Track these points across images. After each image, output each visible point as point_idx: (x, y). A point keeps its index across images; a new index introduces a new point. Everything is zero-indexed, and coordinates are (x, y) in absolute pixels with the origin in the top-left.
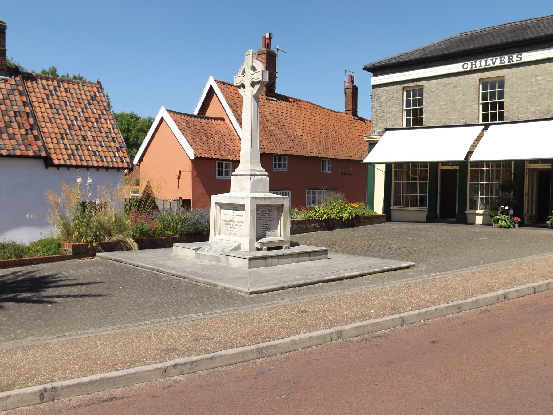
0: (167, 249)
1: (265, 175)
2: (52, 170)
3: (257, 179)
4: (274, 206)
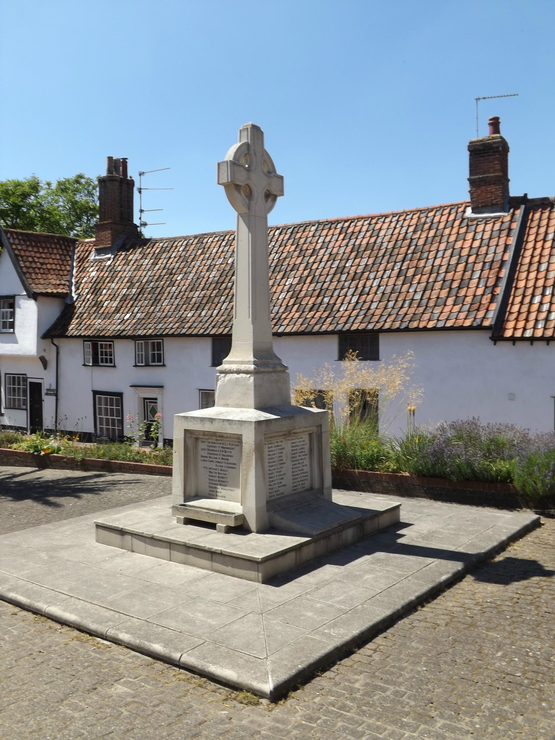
0: (345, 492)
1: (247, 372)
2: (504, 347)
3: (229, 381)
4: (227, 438)
